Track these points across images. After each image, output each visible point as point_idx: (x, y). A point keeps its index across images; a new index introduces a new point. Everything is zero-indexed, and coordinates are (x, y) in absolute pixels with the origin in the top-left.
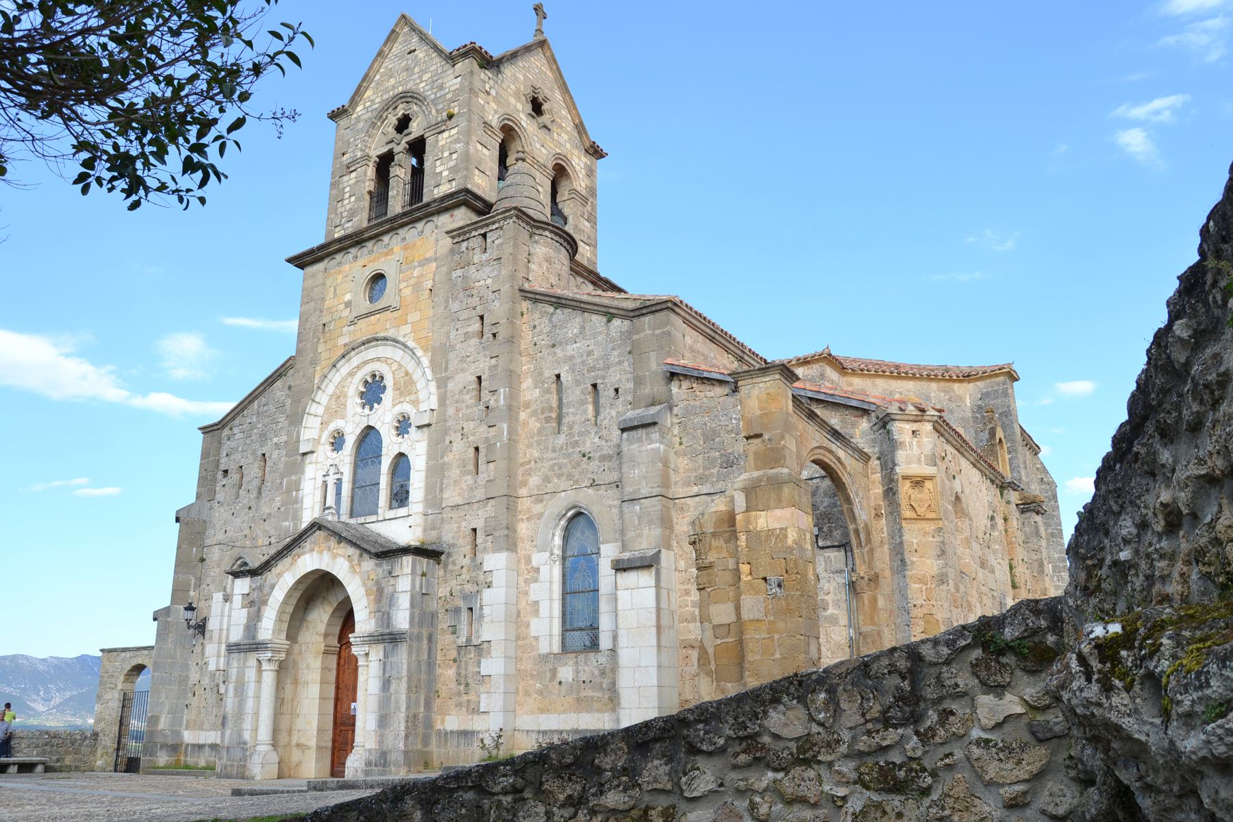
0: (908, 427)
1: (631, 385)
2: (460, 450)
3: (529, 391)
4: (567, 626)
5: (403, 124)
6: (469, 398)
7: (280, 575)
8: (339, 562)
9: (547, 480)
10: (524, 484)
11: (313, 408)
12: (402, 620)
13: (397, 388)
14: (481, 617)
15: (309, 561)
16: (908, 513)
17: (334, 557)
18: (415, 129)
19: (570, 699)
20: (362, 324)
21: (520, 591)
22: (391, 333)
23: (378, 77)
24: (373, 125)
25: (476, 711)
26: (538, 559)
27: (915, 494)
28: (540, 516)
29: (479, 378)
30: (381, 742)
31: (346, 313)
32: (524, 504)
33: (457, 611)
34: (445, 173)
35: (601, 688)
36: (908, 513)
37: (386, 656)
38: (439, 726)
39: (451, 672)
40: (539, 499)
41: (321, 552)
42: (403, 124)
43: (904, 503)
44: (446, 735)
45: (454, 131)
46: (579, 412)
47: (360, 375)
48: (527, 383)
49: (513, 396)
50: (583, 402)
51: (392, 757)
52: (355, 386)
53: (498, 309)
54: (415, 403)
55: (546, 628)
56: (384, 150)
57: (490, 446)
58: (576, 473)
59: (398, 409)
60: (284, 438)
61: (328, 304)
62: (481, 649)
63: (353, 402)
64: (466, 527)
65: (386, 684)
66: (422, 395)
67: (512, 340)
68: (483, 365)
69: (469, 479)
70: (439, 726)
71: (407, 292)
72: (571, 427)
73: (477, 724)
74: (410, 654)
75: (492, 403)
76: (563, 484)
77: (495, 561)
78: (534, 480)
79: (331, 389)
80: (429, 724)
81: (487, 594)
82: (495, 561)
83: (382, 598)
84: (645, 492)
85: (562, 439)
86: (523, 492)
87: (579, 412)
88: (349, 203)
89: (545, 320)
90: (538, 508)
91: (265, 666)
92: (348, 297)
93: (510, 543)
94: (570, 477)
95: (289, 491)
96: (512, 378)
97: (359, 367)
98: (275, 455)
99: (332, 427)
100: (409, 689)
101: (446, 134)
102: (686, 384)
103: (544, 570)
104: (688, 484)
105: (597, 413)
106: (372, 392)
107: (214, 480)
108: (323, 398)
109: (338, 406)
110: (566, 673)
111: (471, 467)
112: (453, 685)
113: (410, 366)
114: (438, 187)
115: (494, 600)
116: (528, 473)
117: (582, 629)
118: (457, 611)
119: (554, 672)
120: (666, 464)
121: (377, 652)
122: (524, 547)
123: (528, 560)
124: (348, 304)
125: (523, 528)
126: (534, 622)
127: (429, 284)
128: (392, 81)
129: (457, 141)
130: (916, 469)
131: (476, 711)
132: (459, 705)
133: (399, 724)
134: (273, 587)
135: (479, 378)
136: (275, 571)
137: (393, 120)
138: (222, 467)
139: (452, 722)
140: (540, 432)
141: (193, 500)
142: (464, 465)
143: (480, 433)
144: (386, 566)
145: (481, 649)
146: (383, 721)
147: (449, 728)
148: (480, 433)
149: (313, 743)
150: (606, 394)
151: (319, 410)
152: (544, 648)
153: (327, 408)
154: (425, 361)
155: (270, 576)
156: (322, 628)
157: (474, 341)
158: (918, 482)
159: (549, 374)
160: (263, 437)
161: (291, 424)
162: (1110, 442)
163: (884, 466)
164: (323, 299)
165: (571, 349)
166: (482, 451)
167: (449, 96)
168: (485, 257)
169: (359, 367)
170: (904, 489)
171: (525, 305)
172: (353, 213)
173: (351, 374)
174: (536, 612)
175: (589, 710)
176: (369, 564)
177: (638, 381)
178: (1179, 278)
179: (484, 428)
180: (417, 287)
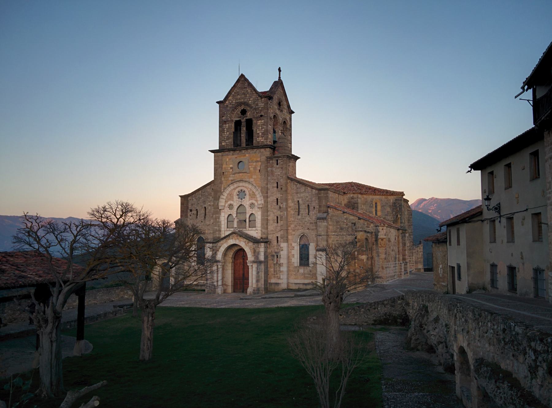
0: (381, 228)
1: (318, 207)
2: (272, 217)
3: (291, 204)
4: (301, 259)
5: (244, 112)
6: (275, 204)
7: (222, 244)
8: (242, 243)
9: (296, 226)
10: (290, 226)
11: (222, 197)
12: (262, 258)
13: (250, 195)
14: (280, 257)
15: (231, 242)
16: (380, 246)
17: (240, 241)
18: (249, 115)
19: (303, 276)
20: (237, 175)
21: (289, 252)
22: (247, 180)
23: (233, 93)
24: (233, 110)
25: (280, 278)
26: (294, 244)
27: (382, 242)
28: (294, 235)
29: (277, 199)
30: (257, 285)
31: (231, 170)
32: (290, 231)
33: (273, 256)
34: (260, 134)
35: (310, 274)
36: (380, 246)
37: (258, 266)
38: (269, 282)
39: (272, 269)
40: (294, 231)
41: (235, 239)
42: (244, 112)
43: (379, 243)
44: (271, 284)
45: (263, 121)
46: (304, 211)
47: (237, 190)
48: (290, 201)
49: (287, 205)
50: (305, 209)
51: (260, 289)
52: (235, 192)
53: (282, 181)
54: (257, 201)
55: (296, 260)
56: (238, 119)
57: (281, 217)
58: (304, 225)
59: (251, 201)
60: (212, 204)
61: (224, 166)
62: (280, 265)
63: (235, 197)
64: (275, 236)
65: (258, 273)
66: (259, 199)
67: (286, 191)
68: (279, 196)
69: (276, 224)
70: (269, 282)
71: (252, 169)
72: (302, 214)
73: (279, 281)
74: (264, 266)
75: (281, 206)
76: (300, 228)
77: (284, 245)
78: (292, 226)
79: (228, 192)
80: (267, 281)
81: (282, 253)
82: (284, 245)
83: (256, 253)
84: (323, 234)
85: (300, 217)
86: (289, 228)
87: (304, 211)
88: (226, 134)
89: (295, 186)
90: (294, 233)
91: (219, 267)
92: (231, 166)
93: (287, 241)
94: (302, 226)
95: (216, 219)
96: (286, 200)
97: (237, 187)
98: (209, 208)
99: (229, 203)
100: (264, 274)
101: (260, 121)
102: (332, 209)
103: (296, 248)
104: (332, 232)
105: (309, 212)
106: (241, 194)
107: (187, 212)
108: (225, 194)
109: (230, 196)
110: (301, 271)
111: (276, 221)
112: (273, 273)
113: (254, 190)
114: (259, 139)
115: (283, 254)
116: (291, 224)
117: (304, 259)
118: (273, 256)
119: (298, 271)
120: (327, 227)
121: (255, 266)
122: (290, 242)
123: (291, 245)
124: (231, 168)
125: (290, 237)
126: (293, 259)
127: (259, 168)
128: (239, 97)
129: (264, 125)
130: (382, 237)
131: (280, 278)
132: (275, 277)
133: (262, 281)
134: (220, 247)
135: (277, 199)
136: (222, 242)
137: (240, 109)
138: (190, 209)
139: (273, 281)
140: (294, 214)
141: (180, 217)
142: (274, 220)
143: (278, 213)
144: (256, 245)
145: (280, 265)
146: (258, 281)
147: (272, 282)
148: (278, 213)
149: (230, 284)
150: (311, 208)
151: (225, 197)
152: (296, 265)
153: (227, 197)
154: (259, 190)
155: (219, 244)
156: (231, 256)
157: (276, 189)
158: (382, 240)
159: (296, 200)
160: (204, 202)
161: (214, 200)
162: (431, 197)
163: (376, 235)
164: (222, 165)
165: (302, 195)
166: (279, 218)
167: (260, 109)
168: (277, 166)
169: (237, 187)
170: (380, 240)
171: (289, 181)
172: (228, 138)
173: (235, 189)
174: (294, 257)
175: (307, 279)
176: (251, 244)
177: (320, 206)
178: (297, 158)
179: (279, 212)
180: (255, 168)
